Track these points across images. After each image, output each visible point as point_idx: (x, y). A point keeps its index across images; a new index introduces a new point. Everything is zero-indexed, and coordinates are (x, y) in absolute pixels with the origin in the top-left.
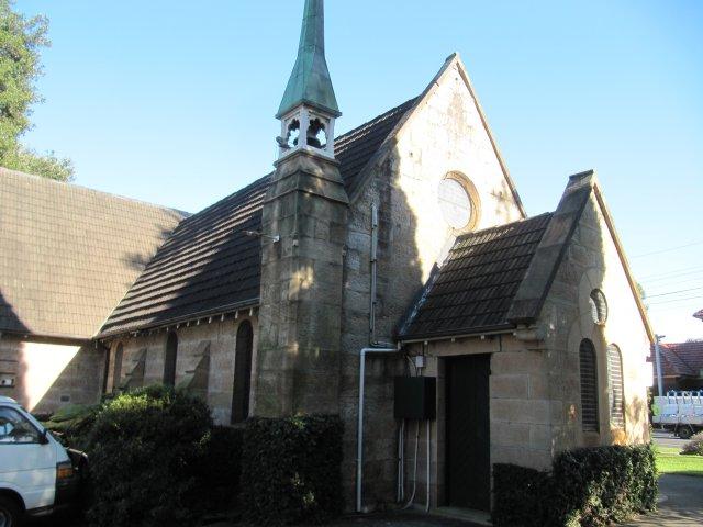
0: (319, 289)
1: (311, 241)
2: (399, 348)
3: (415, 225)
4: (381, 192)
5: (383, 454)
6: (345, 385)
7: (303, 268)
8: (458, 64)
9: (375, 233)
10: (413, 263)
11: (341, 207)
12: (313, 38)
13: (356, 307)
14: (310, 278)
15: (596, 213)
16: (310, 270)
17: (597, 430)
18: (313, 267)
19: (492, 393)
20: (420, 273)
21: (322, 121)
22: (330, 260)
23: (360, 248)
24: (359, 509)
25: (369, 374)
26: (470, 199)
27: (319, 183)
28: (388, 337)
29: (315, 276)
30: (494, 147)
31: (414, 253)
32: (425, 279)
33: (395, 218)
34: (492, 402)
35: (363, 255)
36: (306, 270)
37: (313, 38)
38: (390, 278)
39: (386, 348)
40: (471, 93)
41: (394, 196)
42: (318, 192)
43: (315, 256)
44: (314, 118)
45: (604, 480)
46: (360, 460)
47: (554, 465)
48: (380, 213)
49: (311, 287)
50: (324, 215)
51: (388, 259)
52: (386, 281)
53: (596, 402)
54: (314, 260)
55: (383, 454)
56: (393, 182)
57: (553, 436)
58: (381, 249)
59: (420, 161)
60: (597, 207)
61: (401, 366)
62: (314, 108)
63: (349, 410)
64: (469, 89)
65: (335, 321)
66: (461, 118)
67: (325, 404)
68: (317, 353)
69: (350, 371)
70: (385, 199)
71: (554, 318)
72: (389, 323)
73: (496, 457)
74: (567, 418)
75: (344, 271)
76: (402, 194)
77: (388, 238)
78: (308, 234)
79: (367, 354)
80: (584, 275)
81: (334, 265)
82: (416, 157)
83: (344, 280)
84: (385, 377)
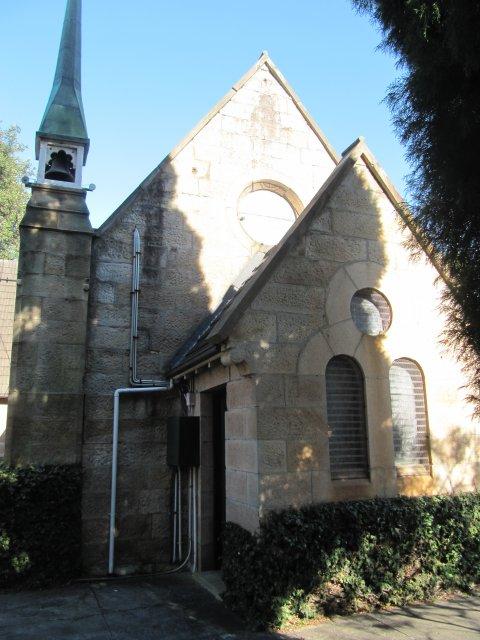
0: (49, 329)
1: (39, 278)
2: (171, 385)
3: (199, 246)
4: (148, 216)
5: (151, 502)
6: (90, 432)
7: (26, 309)
8: (266, 63)
9: (138, 261)
10: (195, 289)
11: (80, 237)
12: (68, 76)
13: (110, 343)
14: (37, 319)
15: (369, 192)
16: (37, 311)
17: (368, 476)
18: (41, 305)
19: (226, 437)
20: (207, 300)
21: (68, 152)
22: (66, 295)
23: (117, 279)
24: (110, 571)
25: (127, 416)
26: (293, 207)
27: (53, 216)
28: (158, 374)
29: (43, 315)
30: (325, 146)
31: (198, 277)
32: (214, 306)
33: (168, 240)
34: (227, 443)
35: (120, 287)
36: (30, 310)
37: (68, 76)
38: (160, 307)
39: (154, 386)
40: (287, 92)
41: (167, 219)
42: (48, 225)
43: (44, 294)
44: (56, 150)
45: (367, 546)
46: (113, 514)
47: (263, 526)
48: (147, 238)
49: (38, 327)
50: (58, 248)
51: (157, 287)
52: (154, 312)
53: (366, 439)
54: (42, 298)
55: (151, 502)
56: (166, 203)
57: (263, 489)
58: (149, 277)
59: (208, 176)
60: (370, 183)
61: (178, 406)
62: (54, 140)
63: (98, 458)
64: (285, 88)
65: (73, 359)
66: (272, 121)
67: (59, 452)
68: (45, 399)
69: (99, 414)
70: (154, 222)
71: (270, 332)
72: (160, 358)
73: (228, 520)
74: (296, 462)
75: (90, 305)
76: (180, 217)
77: (157, 262)
78: (35, 270)
79: (121, 395)
80: (339, 275)
81: (73, 300)
82: (201, 173)
83: (91, 316)
84: (153, 419)
